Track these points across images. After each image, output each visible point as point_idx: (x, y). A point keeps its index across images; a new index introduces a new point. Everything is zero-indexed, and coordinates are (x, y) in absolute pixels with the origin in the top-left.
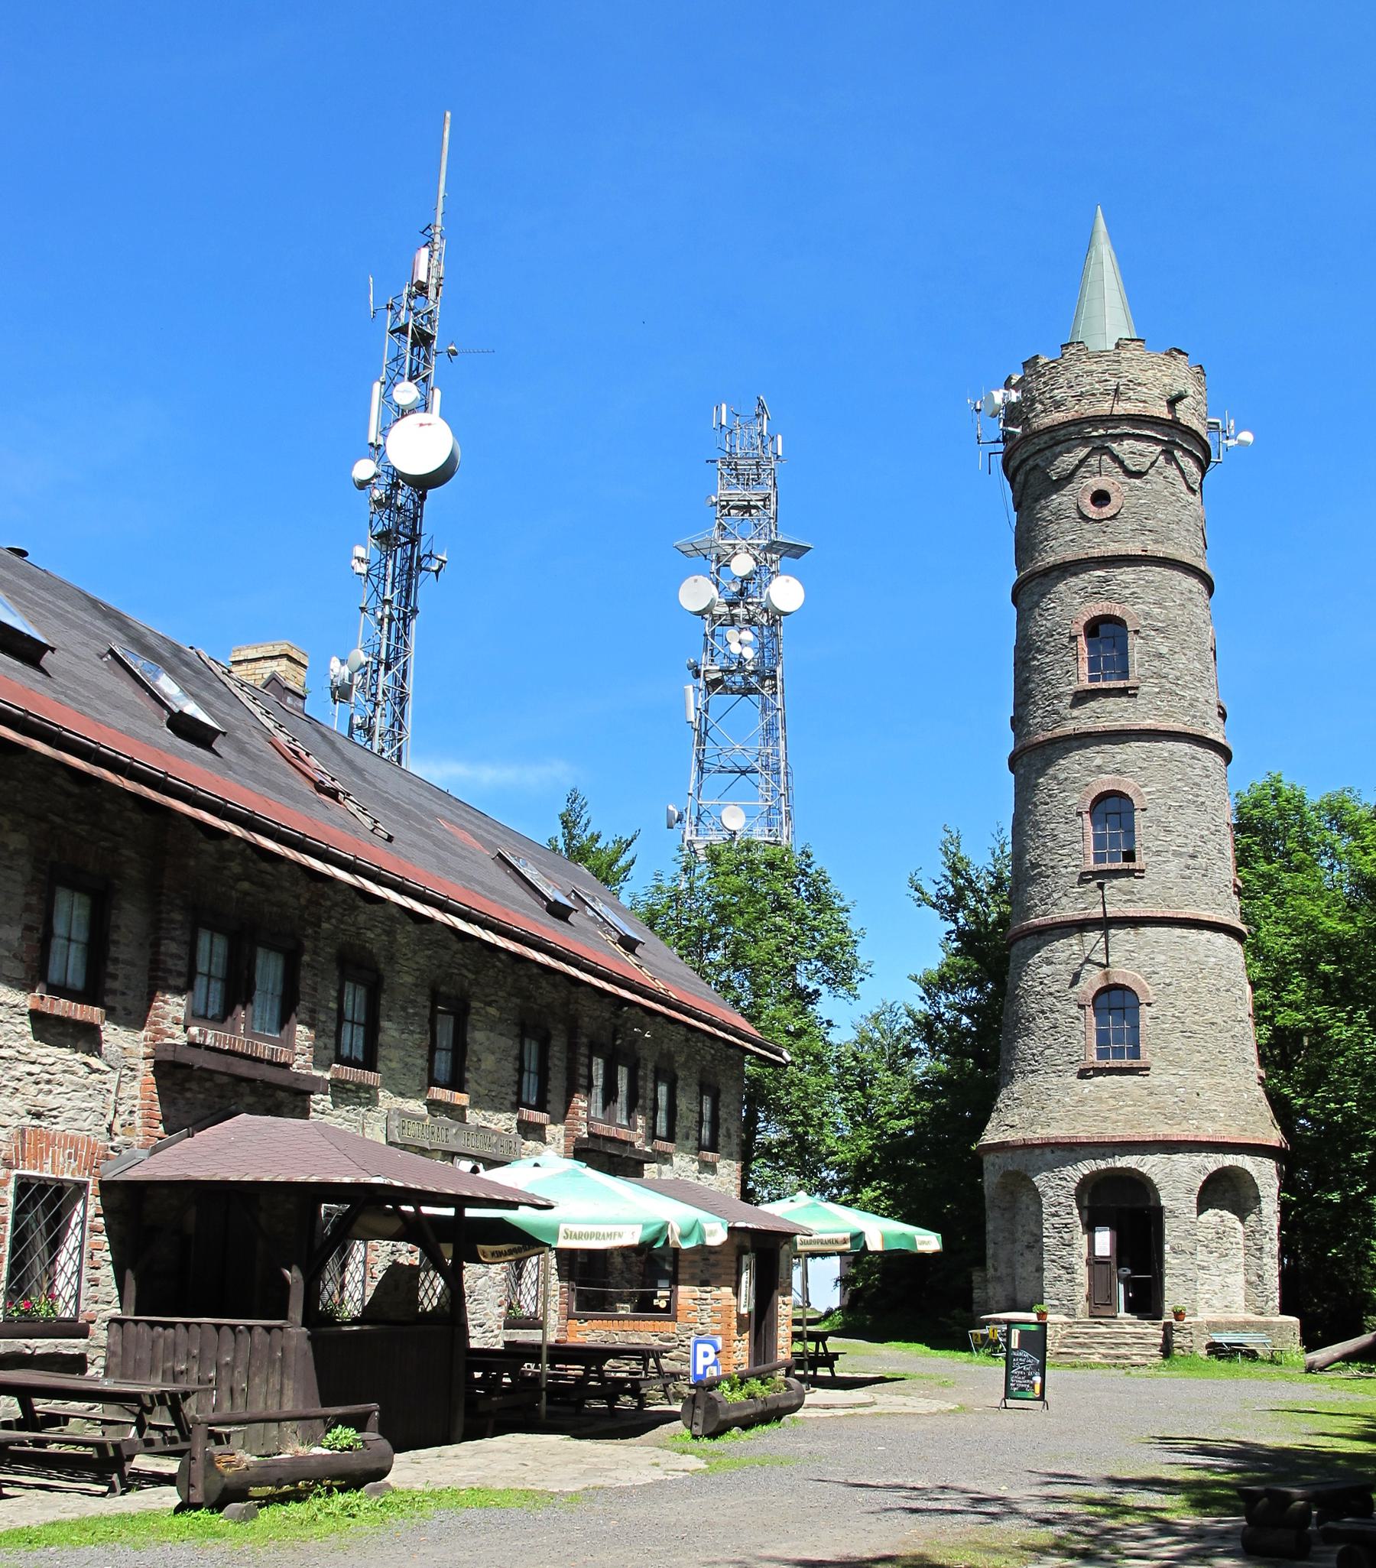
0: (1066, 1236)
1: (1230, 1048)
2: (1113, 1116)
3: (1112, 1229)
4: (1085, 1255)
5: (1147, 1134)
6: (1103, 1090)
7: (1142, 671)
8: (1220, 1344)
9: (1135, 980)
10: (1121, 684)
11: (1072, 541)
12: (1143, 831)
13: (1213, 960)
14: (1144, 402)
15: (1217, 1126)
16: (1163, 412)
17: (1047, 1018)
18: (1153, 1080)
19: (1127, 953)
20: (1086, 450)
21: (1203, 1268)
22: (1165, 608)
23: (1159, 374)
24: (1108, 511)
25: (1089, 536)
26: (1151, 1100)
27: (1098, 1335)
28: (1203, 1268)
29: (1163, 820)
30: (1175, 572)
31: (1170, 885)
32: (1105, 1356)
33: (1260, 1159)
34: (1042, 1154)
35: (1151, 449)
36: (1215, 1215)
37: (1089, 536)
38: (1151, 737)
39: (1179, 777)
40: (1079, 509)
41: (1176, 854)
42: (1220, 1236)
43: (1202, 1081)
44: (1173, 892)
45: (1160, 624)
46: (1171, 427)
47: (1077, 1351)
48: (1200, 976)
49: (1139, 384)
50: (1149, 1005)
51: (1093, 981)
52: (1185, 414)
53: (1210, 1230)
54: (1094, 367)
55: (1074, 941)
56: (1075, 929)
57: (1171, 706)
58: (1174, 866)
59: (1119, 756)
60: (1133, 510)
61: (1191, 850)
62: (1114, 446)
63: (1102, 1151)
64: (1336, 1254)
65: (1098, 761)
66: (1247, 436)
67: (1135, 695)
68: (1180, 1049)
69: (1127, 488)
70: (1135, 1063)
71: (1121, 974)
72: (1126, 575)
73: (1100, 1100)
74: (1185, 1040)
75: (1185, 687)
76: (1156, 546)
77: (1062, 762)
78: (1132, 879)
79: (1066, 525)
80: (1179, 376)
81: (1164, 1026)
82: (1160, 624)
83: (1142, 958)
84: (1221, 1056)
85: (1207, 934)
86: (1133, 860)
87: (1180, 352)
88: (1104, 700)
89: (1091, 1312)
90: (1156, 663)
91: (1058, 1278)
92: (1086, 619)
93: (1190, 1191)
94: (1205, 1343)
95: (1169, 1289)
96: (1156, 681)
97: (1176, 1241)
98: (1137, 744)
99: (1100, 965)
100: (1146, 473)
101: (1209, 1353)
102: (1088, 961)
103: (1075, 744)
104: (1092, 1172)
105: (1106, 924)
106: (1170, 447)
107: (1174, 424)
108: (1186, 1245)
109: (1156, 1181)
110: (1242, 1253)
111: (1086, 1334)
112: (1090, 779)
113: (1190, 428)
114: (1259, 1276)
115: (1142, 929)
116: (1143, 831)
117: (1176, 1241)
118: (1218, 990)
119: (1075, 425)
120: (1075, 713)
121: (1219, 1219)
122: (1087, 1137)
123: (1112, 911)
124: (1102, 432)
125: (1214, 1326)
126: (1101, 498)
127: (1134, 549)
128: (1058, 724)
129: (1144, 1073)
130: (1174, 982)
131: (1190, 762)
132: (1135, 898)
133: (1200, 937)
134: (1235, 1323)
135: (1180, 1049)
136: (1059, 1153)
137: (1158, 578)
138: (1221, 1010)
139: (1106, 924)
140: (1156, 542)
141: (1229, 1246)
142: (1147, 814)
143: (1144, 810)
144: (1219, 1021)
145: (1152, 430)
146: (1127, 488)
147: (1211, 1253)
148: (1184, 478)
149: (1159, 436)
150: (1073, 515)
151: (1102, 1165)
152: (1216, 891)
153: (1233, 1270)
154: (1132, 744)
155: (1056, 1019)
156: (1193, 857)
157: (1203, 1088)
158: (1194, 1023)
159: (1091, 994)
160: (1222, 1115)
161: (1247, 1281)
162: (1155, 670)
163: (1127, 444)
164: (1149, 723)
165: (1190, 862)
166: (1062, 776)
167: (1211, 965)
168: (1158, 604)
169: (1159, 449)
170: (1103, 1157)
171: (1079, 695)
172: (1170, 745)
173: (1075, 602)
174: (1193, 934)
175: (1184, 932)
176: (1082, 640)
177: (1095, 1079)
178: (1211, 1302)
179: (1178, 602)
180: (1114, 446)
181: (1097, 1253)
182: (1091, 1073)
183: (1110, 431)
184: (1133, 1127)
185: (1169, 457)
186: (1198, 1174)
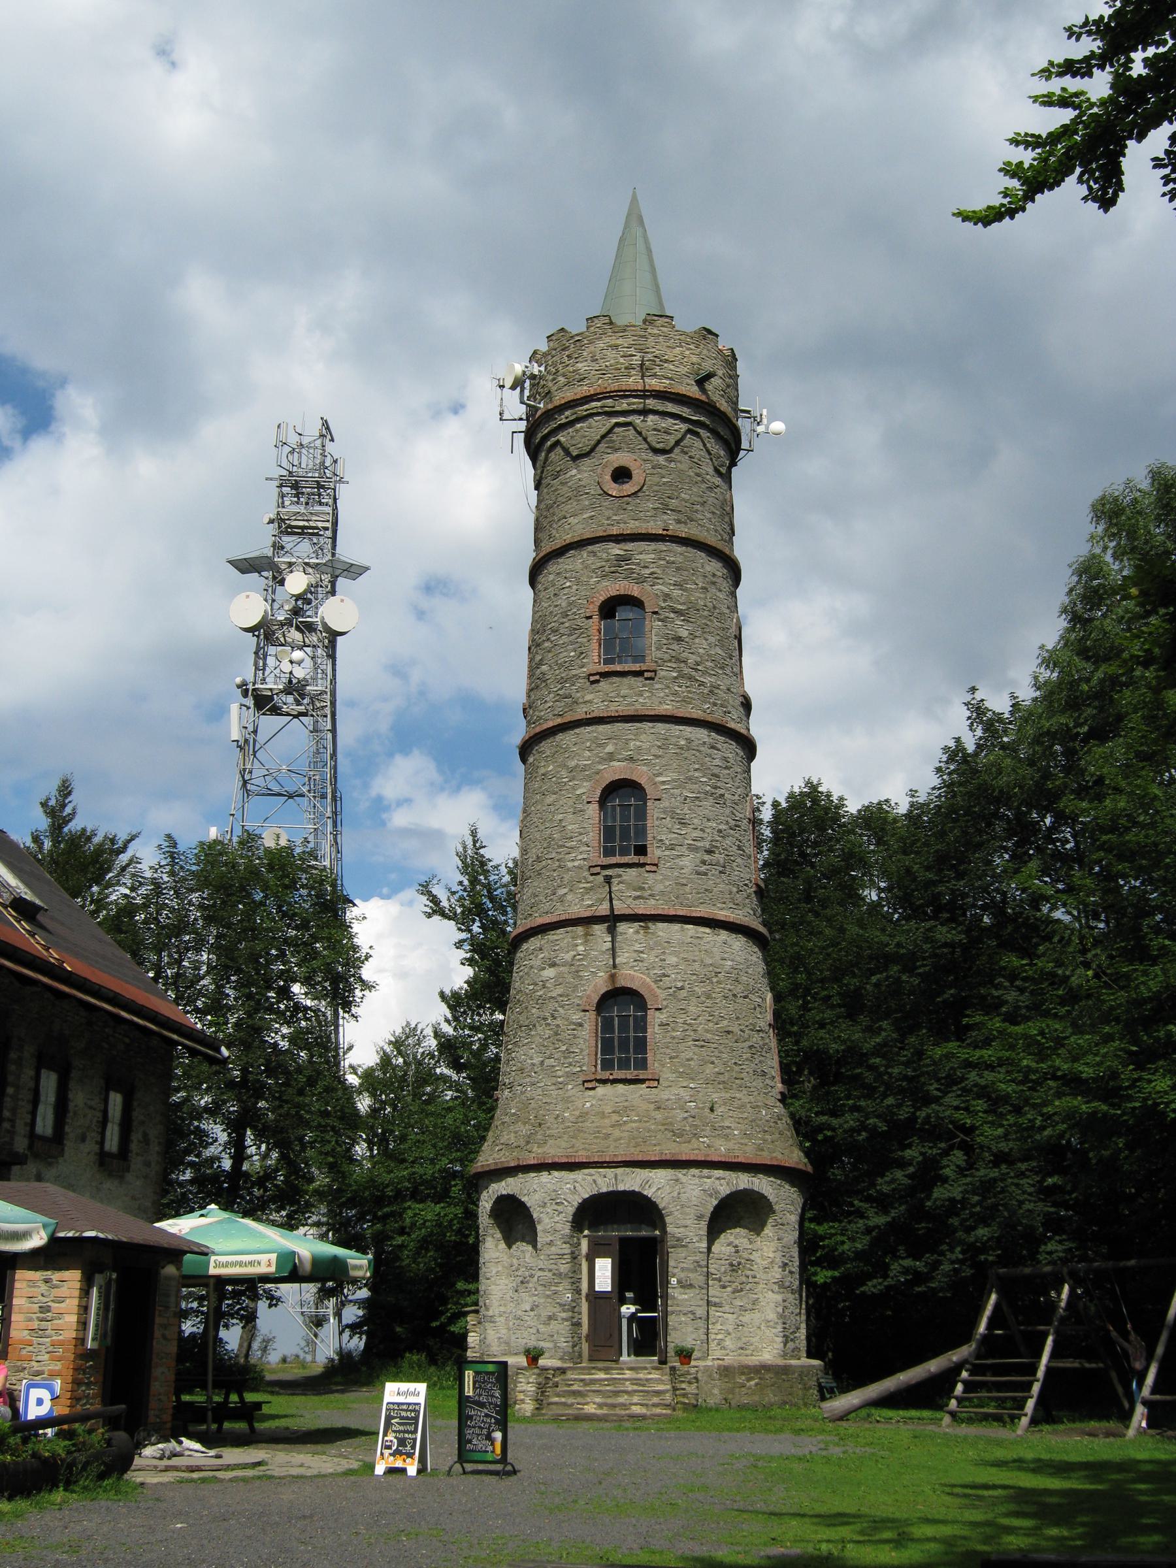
2: (617, 1133)
6: (606, 1105)
7: (659, 654)
13: (730, 963)
16: (693, 391)
19: (635, 955)
22: (685, 590)
24: (629, 488)
26: (658, 1115)
29: (679, 812)
31: (684, 881)
35: (676, 427)
39: (697, 766)
44: (688, 889)
48: (715, 980)
49: (666, 361)
53: (723, 1262)
60: (656, 488)
68: (692, 1059)
71: (633, 976)
74: (697, 1050)
75: (705, 673)
83: (652, 959)
84: (737, 1068)
90: (675, 646)
92: (602, 599)
93: (700, 1217)
96: (674, 665)
111: (582, 1380)
118: (734, 995)
122: (587, 1157)
126: (621, 475)
132: (646, 894)
135: (692, 1059)
140: (679, 522)
141: (744, 1279)
144: (736, 1029)
147: (724, 1287)
158: (707, 1031)
160: (736, 1132)
165: (707, 857)
167: (727, 968)
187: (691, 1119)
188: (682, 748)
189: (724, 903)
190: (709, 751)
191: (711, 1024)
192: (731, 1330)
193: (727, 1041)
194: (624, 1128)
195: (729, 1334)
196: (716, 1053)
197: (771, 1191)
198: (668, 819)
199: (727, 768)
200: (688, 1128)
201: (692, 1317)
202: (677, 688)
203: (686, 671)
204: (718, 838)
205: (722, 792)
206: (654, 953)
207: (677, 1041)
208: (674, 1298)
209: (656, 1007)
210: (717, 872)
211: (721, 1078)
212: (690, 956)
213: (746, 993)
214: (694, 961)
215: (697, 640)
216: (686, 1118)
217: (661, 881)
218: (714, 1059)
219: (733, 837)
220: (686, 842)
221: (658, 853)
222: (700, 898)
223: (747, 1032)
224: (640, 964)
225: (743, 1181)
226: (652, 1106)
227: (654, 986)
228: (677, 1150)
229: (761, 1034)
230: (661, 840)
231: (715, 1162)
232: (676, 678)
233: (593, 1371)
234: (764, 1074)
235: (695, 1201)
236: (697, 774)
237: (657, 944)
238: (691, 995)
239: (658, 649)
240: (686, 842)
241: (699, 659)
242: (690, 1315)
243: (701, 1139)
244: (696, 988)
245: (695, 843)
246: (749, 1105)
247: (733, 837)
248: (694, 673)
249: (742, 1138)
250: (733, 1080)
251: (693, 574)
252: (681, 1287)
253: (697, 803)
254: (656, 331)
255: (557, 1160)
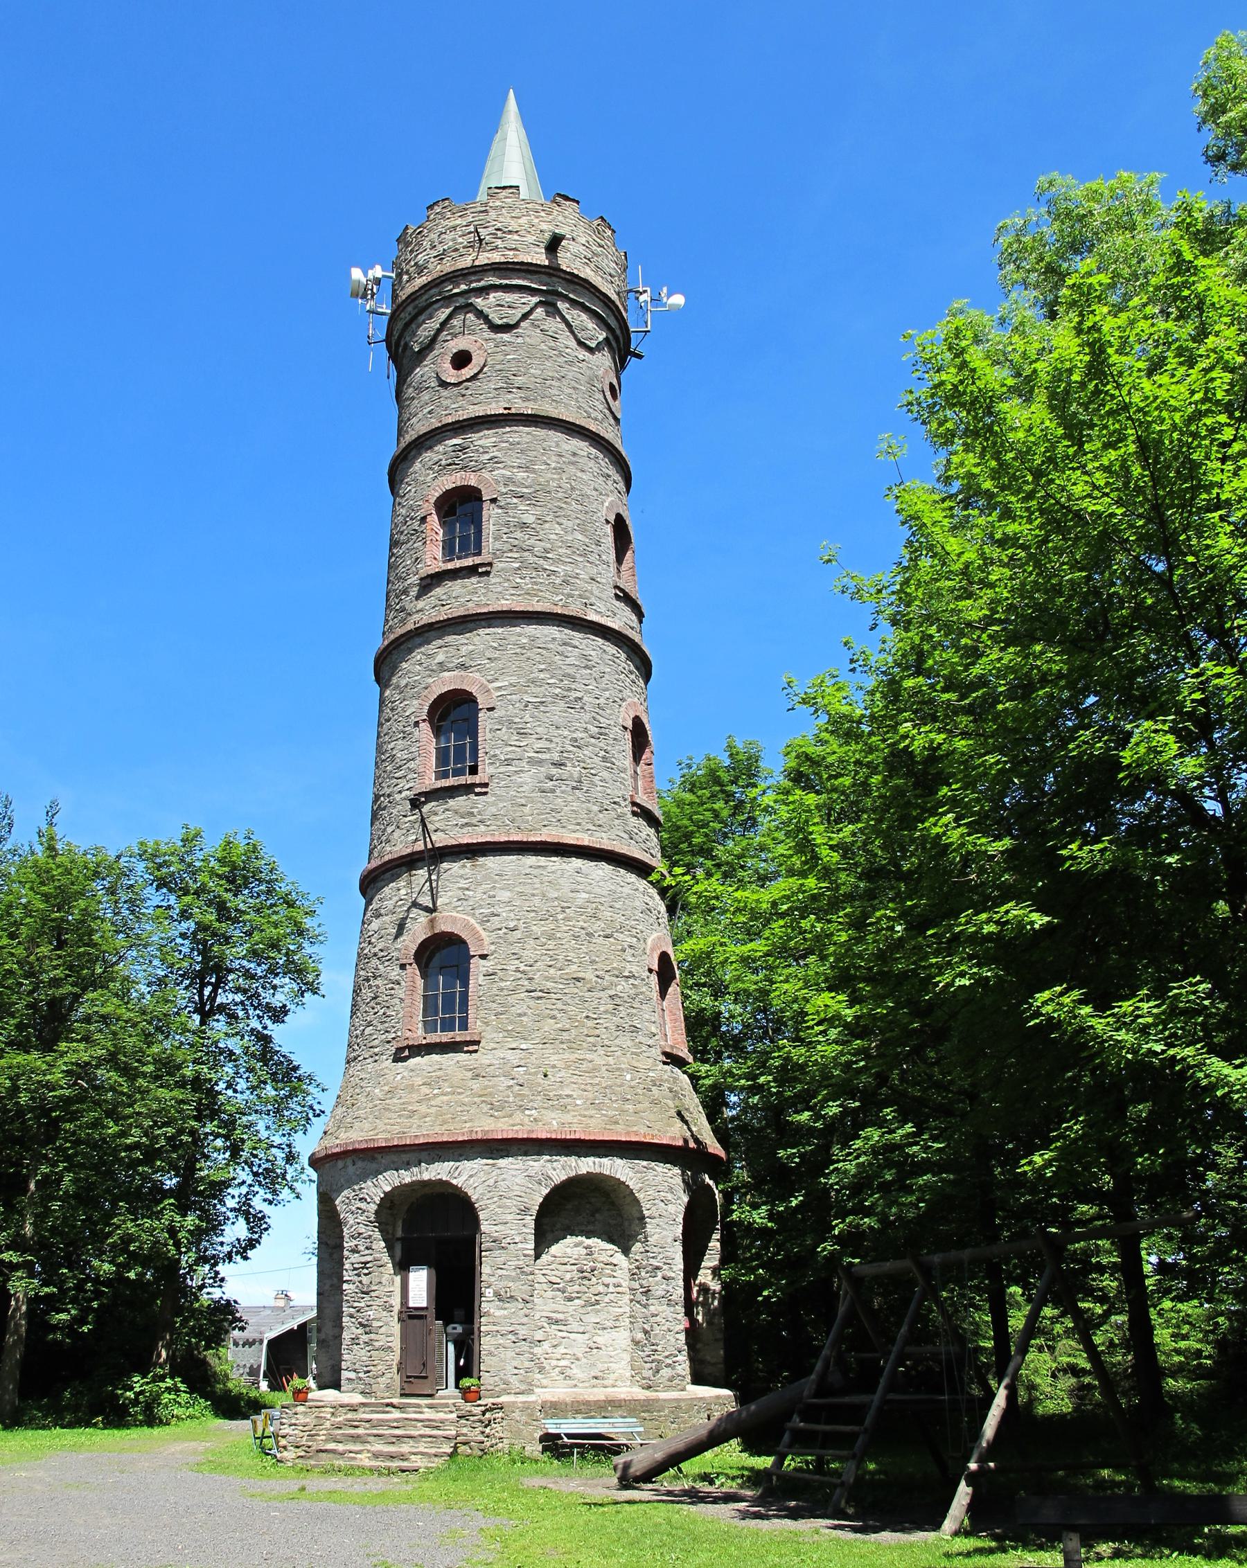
0: (365, 1280)
1: (606, 1012)
2: (423, 1109)
3: (430, 1266)
4: (397, 1307)
5: (460, 1132)
6: (418, 1075)
7: (498, 545)
8: (558, 1436)
9: (467, 925)
10: (468, 562)
11: (430, 412)
12: (488, 736)
13: (585, 895)
14: (515, 249)
15: (568, 1118)
16: (541, 259)
17: (370, 987)
18: (482, 1058)
19: (460, 893)
20: (448, 311)
21: (557, 1322)
22: (534, 471)
23: (536, 221)
24: (467, 372)
25: (445, 403)
26: (476, 1085)
27: (381, 1423)
28: (557, 1322)
29: (517, 720)
30: (551, 433)
31: (523, 801)
32: (376, 1456)
33: (645, 1163)
34: (345, 1167)
35: (523, 300)
36: (576, 1245)
37: (448, 402)
38: (506, 621)
39: (543, 667)
40: (438, 378)
41: (531, 761)
42: (585, 1275)
43: (555, 1057)
44: (527, 810)
45: (525, 490)
46: (550, 275)
47: (341, 1447)
48: (560, 916)
49: (510, 232)
50: (483, 957)
51: (418, 930)
52: (566, 261)
53: (568, 1267)
54: (459, 221)
55: (403, 884)
56: (404, 869)
57: (536, 583)
58: (529, 778)
59: (464, 648)
60: (498, 367)
61: (556, 757)
62: (479, 302)
63: (405, 1157)
64: (769, 1297)
65: (440, 657)
66: (678, 300)
67: (487, 573)
68: (525, 1014)
69: (492, 345)
70: (459, 1036)
71: (452, 919)
72: (485, 439)
73: (411, 1088)
74: (532, 1003)
76: (526, 404)
77: (404, 665)
78: (472, 796)
79: (425, 396)
80: (566, 220)
81: (503, 984)
82: (525, 490)
83: (479, 895)
84: (590, 1023)
85: (577, 863)
86: (476, 773)
87: (567, 198)
88: (450, 584)
89: (402, 1389)
90: (518, 535)
91: (355, 1341)
92: (437, 495)
93: (525, 1211)
94: (537, 1435)
95: (491, 1354)
96: (516, 555)
97: (503, 1284)
98: (488, 631)
99: (427, 909)
100: (516, 326)
101: (545, 1449)
102: (415, 904)
103: (418, 640)
104: (395, 1189)
105: (437, 856)
106: (550, 298)
107: (553, 271)
108: (518, 1289)
109: (474, 1198)
110: (627, 1297)
111: (368, 1421)
112: (430, 680)
113: (577, 276)
114: (646, 1332)
115: (482, 860)
116: (488, 736)
117: (503, 1284)
118: (590, 935)
119: (437, 285)
120: (421, 604)
121: (585, 1251)
122: (386, 1140)
123: (440, 840)
124: (463, 287)
125: (554, 1409)
126: (462, 359)
127: (496, 409)
128: (403, 621)
129: (471, 1048)
130: (521, 925)
131: (560, 649)
132: (474, 821)
133: (564, 866)
134: (587, 1403)
135: (525, 1014)
136: (360, 1164)
137: (527, 439)
138: (593, 962)
139: (437, 856)
140: (527, 399)
141: (601, 1288)
142: (495, 714)
143: (490, 709)
144: (590, 975)
145: (524, 279)
146: (492, 345)
147: (571, 1299)
148: (572, 332)
149: (533, 286)
150: (433, 385)
151: (407, 1177)
152: (596, 808)
153: (609, 1324)
154: (481, 631)
155: (378, 987)
156: (559, 765)
157: (554, 1067)
158: (547, 979)
159: (413, 948)
160: (578, 1102)
161: (633, 1341)
162: (516, 542)
163: (493, 297)
164: (505, 604)
166: (403, 683)
167: (580, 902)
168: (527, 469)
169: (535, 300)
170: (407, 1166)
171: (424, 583)
172: (532, 630)
173: (429, 479)
174: (555, 863)
175: (542, 860)
176: (434, 520)
177: (412, 1061)
178: (568, 1372)
179: (553, 465)
180: (479, 302)
181: (411, 1304)
182: (406, 1053)
183: (474, 285)
184: (444, 1122)
185: (551, 309)
186: (536, 1187)
187: (518, 1088)
188: (524, 648)
189: (579, 824)
190: (560, 649)
191: (552, 971)
192: (580, 1355)
193: (576, 990)
194: (433, 1103)
195: (578, 1359)
196: (559, 1005)
197: (631, 1174)
198: (504, 730)
199: (586, 667)
200: (511, 1099)
201: (513, 1338)
202: (518, 580)
203: (532, 559)
204: (572, 748)
205: (579, 695)
206: (480, 890)
207: (506, 992)
208: (488, 1314)
209: (480, 953)
210: (569, 789)
211: (565, 1036)
212: (528, 890)
213: (609, 932)
214: (533, 895)
215: (547, 526)
216: (510, 1087)
217: (494, 804)
218: (555, 1012)
219: (594, 745)
220: (527, 754)
221: (490, 770)
222: (543, 820)
223: (607, 978)
224: (465, 903)
225: (587, 1165)
226: (470, 1074)
227: (477, 926)
228: (492, 1127)
229: (631, 981)
230: (495, 756)
231: (541, 1140)
232: (519, 569)
233: (388, 1409)
234: (635, 1029)
235: (517, 1190)
236: (542, 676)
237: (487, 878)
238: (527, 937)
239: (496, 539)
240: (527, 754)
241: (549, 546)
242: (510, 1336)
243: (527, 1112)
244: (534, 928)
245: (539, 755)
246: (604, 1068)
247: (594, 745)
248: (541, 562)
249: (586, 1109)
250: (583, 1038)
251: (543, 454)
252: (500, 1300)
253: (542, 708)
254: (498, 203)
255: (357, 1146)
